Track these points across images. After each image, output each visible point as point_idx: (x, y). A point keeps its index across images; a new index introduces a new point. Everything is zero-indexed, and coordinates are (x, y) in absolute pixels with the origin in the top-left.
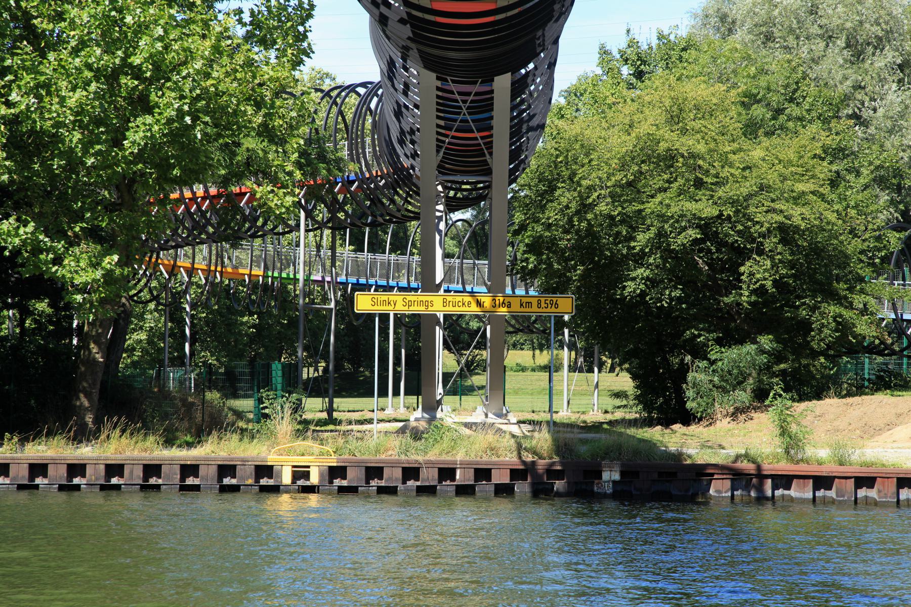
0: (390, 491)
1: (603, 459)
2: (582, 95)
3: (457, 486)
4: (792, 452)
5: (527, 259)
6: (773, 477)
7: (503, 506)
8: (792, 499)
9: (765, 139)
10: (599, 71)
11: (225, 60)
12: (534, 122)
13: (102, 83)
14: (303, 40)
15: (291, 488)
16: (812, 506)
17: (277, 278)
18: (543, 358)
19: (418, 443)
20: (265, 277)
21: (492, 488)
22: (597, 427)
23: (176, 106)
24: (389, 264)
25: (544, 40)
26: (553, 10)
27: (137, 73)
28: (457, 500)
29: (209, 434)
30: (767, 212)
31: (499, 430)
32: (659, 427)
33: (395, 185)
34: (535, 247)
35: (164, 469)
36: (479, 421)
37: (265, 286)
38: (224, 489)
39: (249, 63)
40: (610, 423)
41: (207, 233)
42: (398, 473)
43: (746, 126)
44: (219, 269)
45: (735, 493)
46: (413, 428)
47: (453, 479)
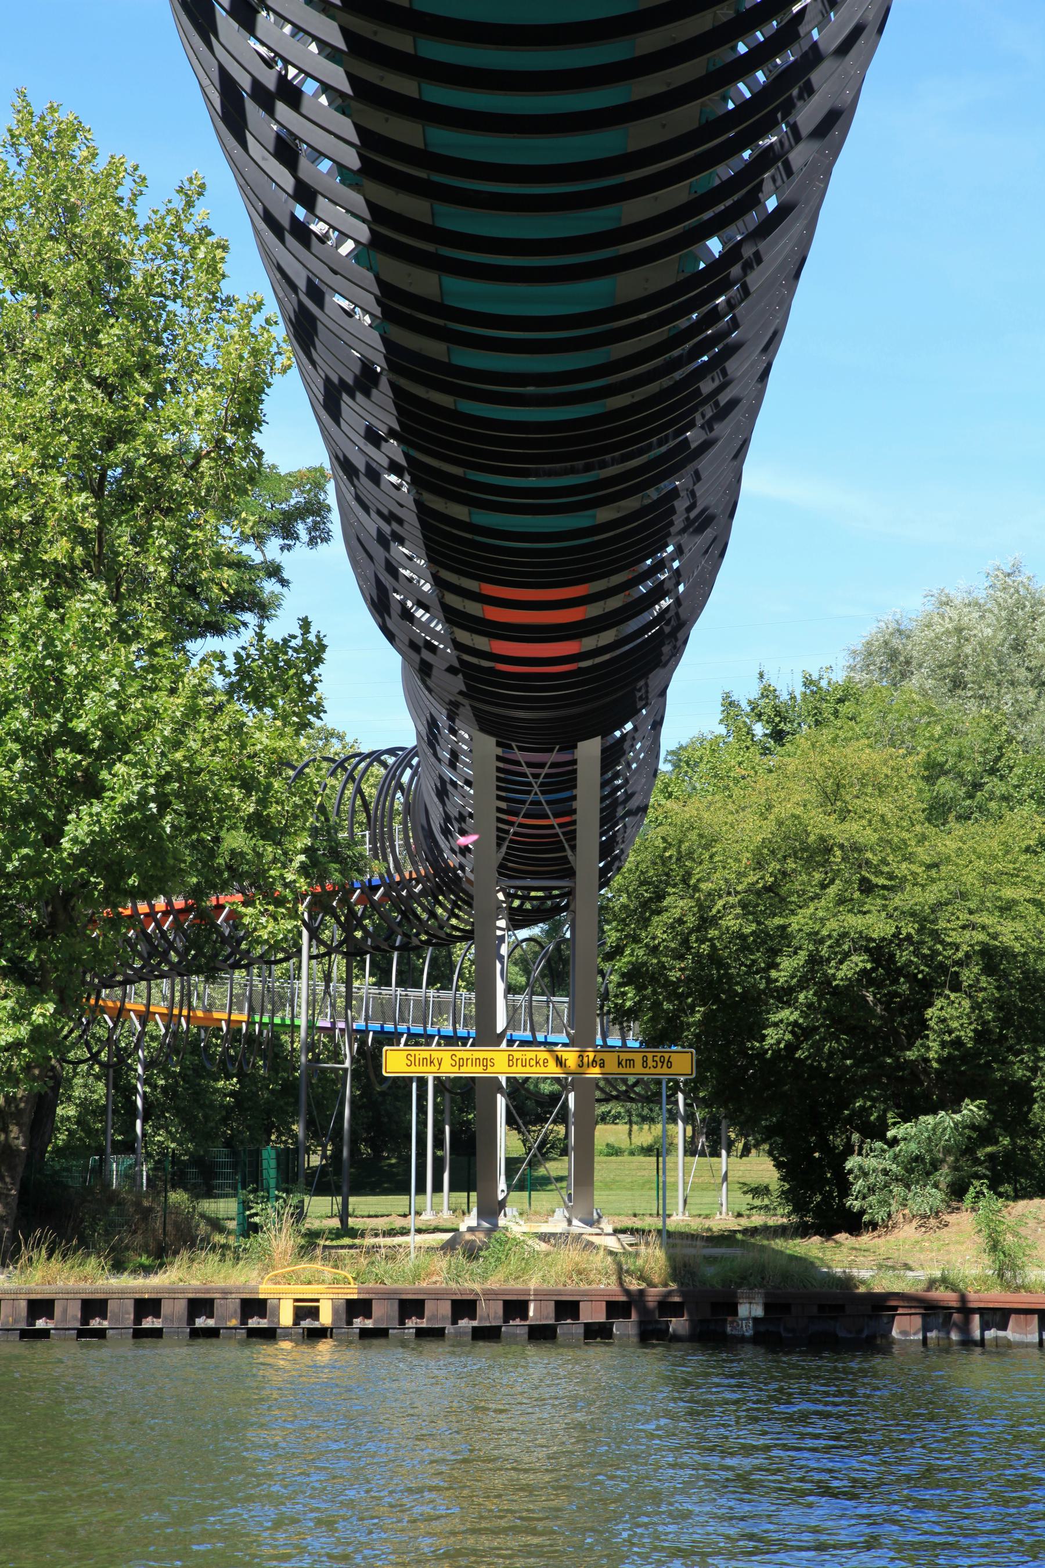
0: (434, 1334)
1: (739, 1285)
2: (696, 764)
3: (530, 1326)
4: (1008, 1274)
5: (624, 994)
6: (981, 1311)
7: (598, 1355)
8: (1009, 1345)
9: (958, 826)
10: (722, 730)
11: (203, 723)
12: (633, 804)
13: (31, 759)
14: (310, 694)
15: (293, 1331)
16: (1036, 1351)
17: (266, 1024)
18: (645, 1135)
19: (474, 1264)
20: (250, 1023)
21: (581, 1330)
22: (726, 1238)
23: (137, 788)
24: (427, 1002)
25: (647, 692)
26: (661, 654)
27: (79, 743)
28: (531, 1350)
29: (176, 1253)
30: (964, 927)
31: (590, 1244)
32: (817, 1239)
33: (436, 892)
34: (634, 976)
35: (111, 1306)
36: (558, 1230)
37: (251, 1039)
38: (196, 1334)
39: (238, 729)
40: (745, 1231)
41: (169, 962)
42: (446, 1309)
43: (932, 807)
44: (185, 1012)
45: (929, 1335)
46: (467, 1242)
47: (525, 1316)
